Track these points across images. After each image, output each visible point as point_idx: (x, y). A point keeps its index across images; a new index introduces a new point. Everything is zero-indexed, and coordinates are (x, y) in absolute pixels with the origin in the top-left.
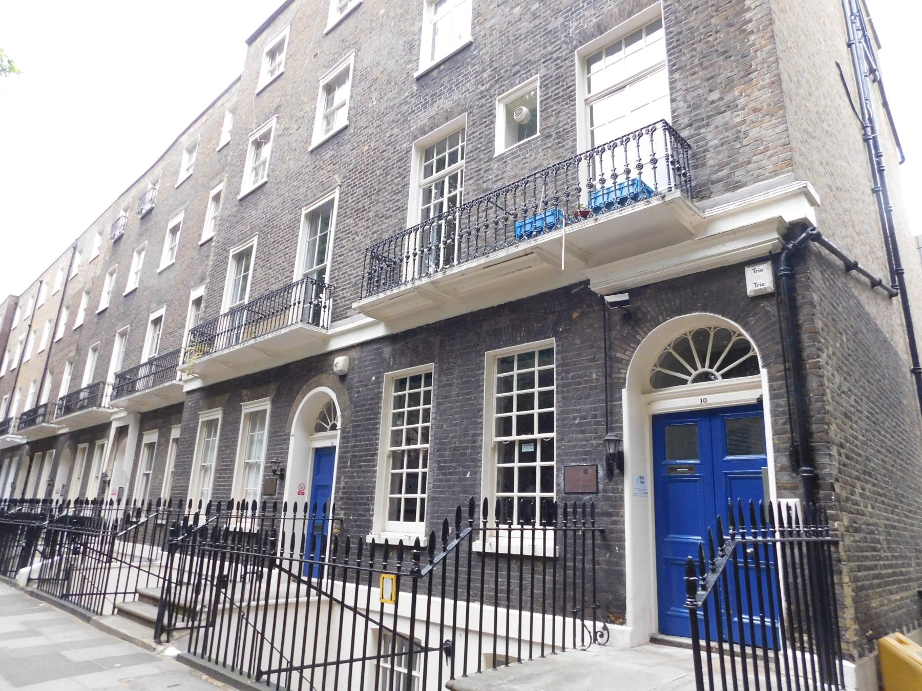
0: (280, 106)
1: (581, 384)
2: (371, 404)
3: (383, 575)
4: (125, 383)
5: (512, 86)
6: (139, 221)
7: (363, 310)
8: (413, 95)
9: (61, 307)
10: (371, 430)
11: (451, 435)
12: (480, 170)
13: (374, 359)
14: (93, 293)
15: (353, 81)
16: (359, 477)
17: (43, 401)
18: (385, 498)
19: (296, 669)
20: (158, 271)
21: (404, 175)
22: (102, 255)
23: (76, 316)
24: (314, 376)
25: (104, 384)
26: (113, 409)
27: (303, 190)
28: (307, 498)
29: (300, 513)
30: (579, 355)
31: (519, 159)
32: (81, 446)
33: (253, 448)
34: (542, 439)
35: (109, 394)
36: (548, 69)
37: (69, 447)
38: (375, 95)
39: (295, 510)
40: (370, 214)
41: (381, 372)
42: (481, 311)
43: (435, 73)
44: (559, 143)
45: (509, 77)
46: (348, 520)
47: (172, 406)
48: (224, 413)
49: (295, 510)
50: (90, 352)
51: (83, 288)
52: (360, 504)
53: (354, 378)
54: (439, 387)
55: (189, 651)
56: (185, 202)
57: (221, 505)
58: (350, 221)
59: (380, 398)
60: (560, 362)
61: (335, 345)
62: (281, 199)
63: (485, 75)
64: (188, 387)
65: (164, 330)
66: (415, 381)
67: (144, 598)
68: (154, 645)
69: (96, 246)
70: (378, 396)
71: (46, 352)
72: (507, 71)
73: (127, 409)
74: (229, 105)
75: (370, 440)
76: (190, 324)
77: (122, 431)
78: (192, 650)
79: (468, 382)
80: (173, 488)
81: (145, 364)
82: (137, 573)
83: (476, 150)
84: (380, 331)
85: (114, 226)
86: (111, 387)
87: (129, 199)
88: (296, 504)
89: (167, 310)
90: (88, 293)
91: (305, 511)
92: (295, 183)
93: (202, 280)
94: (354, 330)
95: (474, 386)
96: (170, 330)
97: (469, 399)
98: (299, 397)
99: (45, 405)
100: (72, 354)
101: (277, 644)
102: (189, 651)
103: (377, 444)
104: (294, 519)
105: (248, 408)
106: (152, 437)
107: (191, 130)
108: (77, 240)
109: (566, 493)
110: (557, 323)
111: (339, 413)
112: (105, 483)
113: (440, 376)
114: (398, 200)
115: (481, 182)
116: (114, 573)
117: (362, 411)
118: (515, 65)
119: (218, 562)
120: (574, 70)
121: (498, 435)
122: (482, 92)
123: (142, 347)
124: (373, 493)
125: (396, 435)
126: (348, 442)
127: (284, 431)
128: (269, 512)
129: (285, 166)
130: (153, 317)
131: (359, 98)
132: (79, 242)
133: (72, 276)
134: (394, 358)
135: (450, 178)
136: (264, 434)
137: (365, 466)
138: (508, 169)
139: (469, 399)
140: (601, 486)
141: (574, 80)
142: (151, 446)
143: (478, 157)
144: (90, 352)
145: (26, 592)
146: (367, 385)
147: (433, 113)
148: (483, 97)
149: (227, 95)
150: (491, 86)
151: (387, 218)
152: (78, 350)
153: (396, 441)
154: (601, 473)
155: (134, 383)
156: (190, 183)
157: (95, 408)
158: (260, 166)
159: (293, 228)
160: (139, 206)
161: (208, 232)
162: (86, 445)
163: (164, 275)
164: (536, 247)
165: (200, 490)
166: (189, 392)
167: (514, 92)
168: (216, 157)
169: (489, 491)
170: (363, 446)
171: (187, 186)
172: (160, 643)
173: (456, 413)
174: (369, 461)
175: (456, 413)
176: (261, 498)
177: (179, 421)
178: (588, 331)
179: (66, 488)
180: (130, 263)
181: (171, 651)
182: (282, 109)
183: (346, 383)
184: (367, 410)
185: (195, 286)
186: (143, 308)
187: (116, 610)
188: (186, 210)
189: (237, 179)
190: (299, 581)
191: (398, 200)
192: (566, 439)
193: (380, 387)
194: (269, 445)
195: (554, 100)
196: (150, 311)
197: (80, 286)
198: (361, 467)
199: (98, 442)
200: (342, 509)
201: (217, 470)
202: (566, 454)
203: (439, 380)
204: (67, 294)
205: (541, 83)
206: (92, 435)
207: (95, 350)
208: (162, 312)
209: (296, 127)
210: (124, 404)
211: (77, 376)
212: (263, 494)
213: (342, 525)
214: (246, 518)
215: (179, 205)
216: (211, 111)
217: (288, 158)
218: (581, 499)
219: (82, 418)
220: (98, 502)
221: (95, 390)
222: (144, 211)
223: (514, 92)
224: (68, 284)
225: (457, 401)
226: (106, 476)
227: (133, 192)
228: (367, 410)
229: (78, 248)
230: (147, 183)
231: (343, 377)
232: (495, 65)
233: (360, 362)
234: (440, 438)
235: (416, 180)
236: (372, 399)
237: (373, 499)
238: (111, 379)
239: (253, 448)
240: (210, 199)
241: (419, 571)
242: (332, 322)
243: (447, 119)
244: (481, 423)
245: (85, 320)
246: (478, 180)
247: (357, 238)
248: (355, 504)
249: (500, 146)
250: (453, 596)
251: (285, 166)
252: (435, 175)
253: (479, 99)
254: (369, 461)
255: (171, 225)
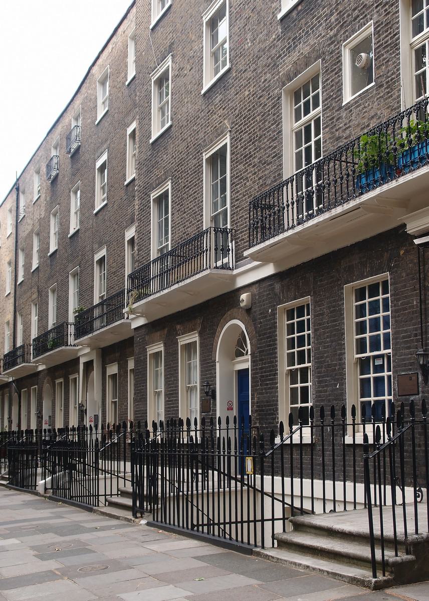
0: (173, 44)
1: (406, 309)
2: (270, 333)
3: (247, 458)
4: (84, 325)
5: (354, 31)
6: (69, 161)
7: (254, 257)
8: (278, 38)
9: (16, 250)
10: (272, 354)
11: (325, 355)
12: (333, 118)
13: (269, 294)
14: (42, 233)
15: (230, 19)
16: (267, 393)
17: (19, 343)
18: (287, 408)
19: (216, 524)
20: (95, 212)
21: (278, 122)
22: (43, 196)
23: (32, 259)
24: (228, 311)
25: (67, 325)
26: (82, 349)
27: (201, 135)
28: (235, 412)
29: (232, 425)
30: (405, 286)
31: (361, 108)
32: (58, 381)
33: (191, 374)
34: (373, 356)
35: (73, 333)
36: (380, 15)
37: (48, 382)
38: (249, 36)
39: (228, 423)
40: (256, 160)
41: (274, 306)
42: (340, 250)
43: (294, 14)
44: (388, 93)
45: (351, 22)
46: (262, 428)
47: (125, 340)
48: (165, 346)
49: (228, 423)
50: (50, 294)
51: (32, 231)
52: (269, 414)
53: (256, 310)
54: (315, 316)
55: (154, 520)
56: (106, 141)
57: (173, 423)
58: (241, 167)
59: (275, 327)
60: (393, 292)
61: (241, 282)
62: (185, 144)
63: (333, 19)
64: (135, 325)
65: (108, 270)
66: (301, 311)
67: (124, 494)
68: (133, 519)
69: (36, 186)
70: (274, 326)
71: (12, 295)
72: (349, 15)
73: (89, 345)
74: (130, 32)
75: (272, 362)
76: (128, 271)
77: (89, 365)
78: (156, 520)
79: (334, 311)
80: (136, 412)
81: (97, 305)
82: (116, 478)
83: (329, 97)
84: (269, 270)
85: (49, 166)
86: (73, 326)
87: (56, 136)
88: (228, 417)
89: (107, 250)
90: (38, 234)
91: (235, 422)
92: (195, 128)
93: (132, 222)
94: (252, 273)
95: (337, 314)
96: (114, 270)
97: (336, 325)
98: (219, 329)
99: (22, 347)
100: (35, 296)
101: (200, 508)
102: (154, 520)
103: (277, 366)
104: (228, 429)
105: (183, 340)
106: (113, 369)
107: (100, 61)
108: (18, 180)
109: (399, 396)
110: (390, 260)
111: (248, 342)
112: (82, 413)
113: (315, 307)
114: (275, 147)
115: (334, 130)
116: (102, 483)
117: (264, 339)
118: (355, 10)
119: (182, 469)
120: (398, 17)
121: (357, 353)
122: (331, 38)
123: (92, 287)
124: (277, 405)
125: (291, 357)
126: (256, 365)
127: (211, 359)
128: (207, 426)
129: (184, 109)
130: (97, 257)
131: (236, 38)
132: (20, 182)
133: (21, 217)
134: (283, 293)
135: (315, 121)
136: (197, 361)
137: (270, 384)
138: (353, 118)
139: (336, 325)
140: (420, 389)
141: (398, 28)
142: (113, 377)
143: (331, 105)
144: (50, 294)
145: (45, 497)
146: (266, 317)
147: (295, 59)
148: (332, 43)
149: (125, 21)
150: (338, 31)
151: (268, 165)
152: (39, 292)
153: (291, 362)
154: (420, 379)
155: (91, 323)
156: (109, 119)
157: (63, 347)
158: (165, 105)
159: (198, 171)
160: (67, 146)
161: (131, 174)
162: (61, 380)
163: (100, 217)
164: (361, 204)
165: (156, 412)
166: (135, 329)
167: (357, 38)
168: (126, 92)
169: (353, 398)
170: (267, 367)
171: (106, 124)
172: (136, 518)
173: (328, 337)
174: (272, 379)
175: (328, 337)
176: (201, 415)
177: (132, 354)
178: (410, 265)
179: (52, 419)
180: (69, 204)
181: (143, 522)
182: (175, 46)
183: (251, 315)
184: (268, 338)
185: (128, 226)
186: (87, 249)
187: (107, 503)
188: (108, 148)
189: (146, 121)
190: (236, 480)
191: (275, 147)
192: (398, 354)
193: (275, 319)
194: (201, 371)
195: (384, 48)
196: (93, 252)
197: (30, 228)
198: (267, 384)
199: (71, 377)
200: (257, 419)
201: (166, 395)
202: (399, 366)
203: (315, 311)
204: (19, 237)
205: (375, 29)
206: (65, 370)
207: (53, 291)
208: (103, 252)
209: (189, 67)
210: (86, 342)
211: (43, 317)
212: (202, 412)
213: (258, 432)
214: (183, 431)
215: (102, 143)
216: (114, 39)
217: (186, 100)
218: (407, 400)
219: (56, 354)
220: (82, 429)
221: (61, 328)
222: (72, 150)
223: (357, 38)
224: (19, 227)
225: (328, 327)
226: (83, 406)
227: (59, 128)
228: (268, 338)
229: (21, 189)
230: (69, 117)
231: (248, 310)
232: (341, 8)
233: (259, 297)
234: (318, 358)
235: (290, 126)
236: (270, 328)
237: (277, 409)
238: (71, 319)
239: (191, 374)
240: (128, 137)
241: (264, 454)
242: (236, 262)
243: (307, 65)
244: (344, 344)
245: (40, 263)
246: (332, 128)
247: (247, 184)
248: (266, 415)
249: (348, 97)
250: (332, 479)
251: (184, 109)
252: (304, 119)
253: (330, 45)
254: (272, 379)
255: (99, 164)
